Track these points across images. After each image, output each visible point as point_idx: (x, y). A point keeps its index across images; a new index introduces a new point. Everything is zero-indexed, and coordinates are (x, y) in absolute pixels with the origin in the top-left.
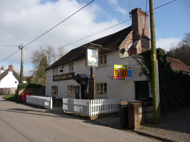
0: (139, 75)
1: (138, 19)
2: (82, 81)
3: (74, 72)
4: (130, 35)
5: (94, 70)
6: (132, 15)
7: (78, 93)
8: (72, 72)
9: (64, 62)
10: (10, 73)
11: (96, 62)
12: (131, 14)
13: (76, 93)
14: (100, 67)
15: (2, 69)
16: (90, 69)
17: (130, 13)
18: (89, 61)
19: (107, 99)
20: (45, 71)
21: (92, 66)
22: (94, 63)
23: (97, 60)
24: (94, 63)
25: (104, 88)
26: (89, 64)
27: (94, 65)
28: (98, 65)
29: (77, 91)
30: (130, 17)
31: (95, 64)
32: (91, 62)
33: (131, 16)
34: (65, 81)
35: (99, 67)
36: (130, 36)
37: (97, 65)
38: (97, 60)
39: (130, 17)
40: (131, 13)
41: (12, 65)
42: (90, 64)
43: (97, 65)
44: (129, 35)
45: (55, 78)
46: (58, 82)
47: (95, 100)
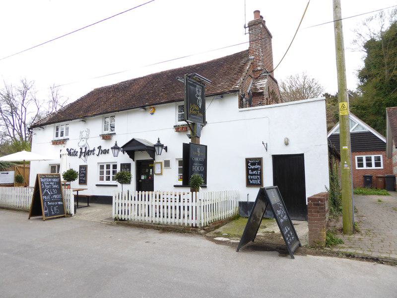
6: (249, 30)
12: (248, 29)
17: (245, 27)
33: (247, 31)
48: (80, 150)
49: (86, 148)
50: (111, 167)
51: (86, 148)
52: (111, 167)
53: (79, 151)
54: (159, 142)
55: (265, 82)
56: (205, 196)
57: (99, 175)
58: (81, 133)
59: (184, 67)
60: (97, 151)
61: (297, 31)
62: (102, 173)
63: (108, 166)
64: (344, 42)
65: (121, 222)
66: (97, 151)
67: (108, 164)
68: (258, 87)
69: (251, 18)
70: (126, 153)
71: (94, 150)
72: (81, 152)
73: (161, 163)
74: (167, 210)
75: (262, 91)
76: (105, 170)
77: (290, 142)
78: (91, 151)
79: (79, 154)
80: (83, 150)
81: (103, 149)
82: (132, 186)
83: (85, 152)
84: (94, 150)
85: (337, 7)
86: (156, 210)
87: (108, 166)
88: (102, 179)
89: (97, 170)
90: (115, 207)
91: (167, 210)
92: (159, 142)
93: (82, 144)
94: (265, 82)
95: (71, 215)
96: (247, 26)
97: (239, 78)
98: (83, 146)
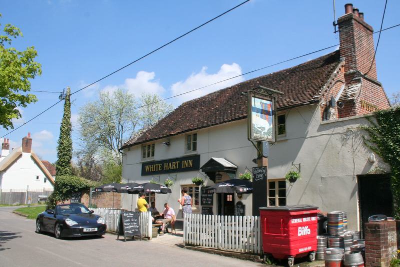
0: (384, 162)
1: (355, 38)
2: (221, 175)
3: (199, 153)
4: (338, 73)
5: (266, 146)
6: (339, 28)
7: (209, 202)
8: (194, 153)
9: (171, 129)
10: (26, 156)
11: (269, 130)
12: (337, 26)
13: (204, 202)
14: (277, 140)
15: (5, 146)
16: (256, 143)
17: (335, 25)
18: (255, 126)
19: (233, 216)
20: (121, 151)
21: (261, 138)
22: (265, 132)
23: (272, 126)
24: (266, 131)
25: (270, 191)
26: (255, 134)
27: (266, 136)
28: (274, 137)
29: (204, 197)
30: (335, 32)
31: (268, 133)
32: (260, 130)
33: (337, 29)
34: (175, 174)
35: (274, 141)
36: (339, 72)
37: (270, 137)
38: (270, 125)
39: (335, 32)
40: (337, 25)
41: (31, 137)
42: (256, 133)
43: (270, 137)
44: (335, 72)
45: (147, 168)
46: (157, 176)
47: (237, 217)
50: (277, 185)
52: (277, 185)
55: (358, 88)
56: (230, 220)
59: (274, 74)
64: (295, 66)
65: (189, 246)
67: (185, 187)
68: (349, 94)
69: (341, 14)
75: (351, 98)
77: (39, 178)
89: (278, 191)
90: (228, 234)
94: (358, 88)
95: (149, 238)
96: (336, 23)
97: (323, 86)
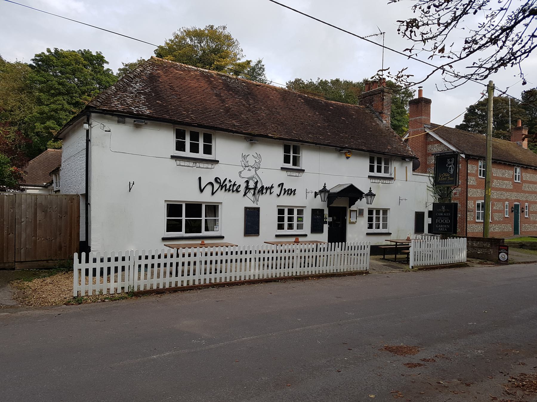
48: (245, 185)
49: (256, 183)
50: (295, 212)
51: (256, 183)
52: (295, 212)
53: (243, 186)
54: (370, 191)
57: (276, 223)
58: (244, 157)
60: (276, 190)
61: (505, 5)
62: (281, 219)
63: (291, 211)
66: (276, 190)
70: (352, 207)
71: (272, 187)
72: (247, 188)
73: (356, 211)
74: (308, 261)
76: (286, 215)
78: (267, 189)
79: (242, 189)
80: (251, 185)
81: (286, 187)
82: (324, 237)
83: (255, 189)
84: (272, 187)
85: (535, 262)
86: (301, 261)
87: (291, 211)
88: (280, 227)
91: (308, 261)
92: (370, 191)
93: (247, 174)
98: (252, 178)
